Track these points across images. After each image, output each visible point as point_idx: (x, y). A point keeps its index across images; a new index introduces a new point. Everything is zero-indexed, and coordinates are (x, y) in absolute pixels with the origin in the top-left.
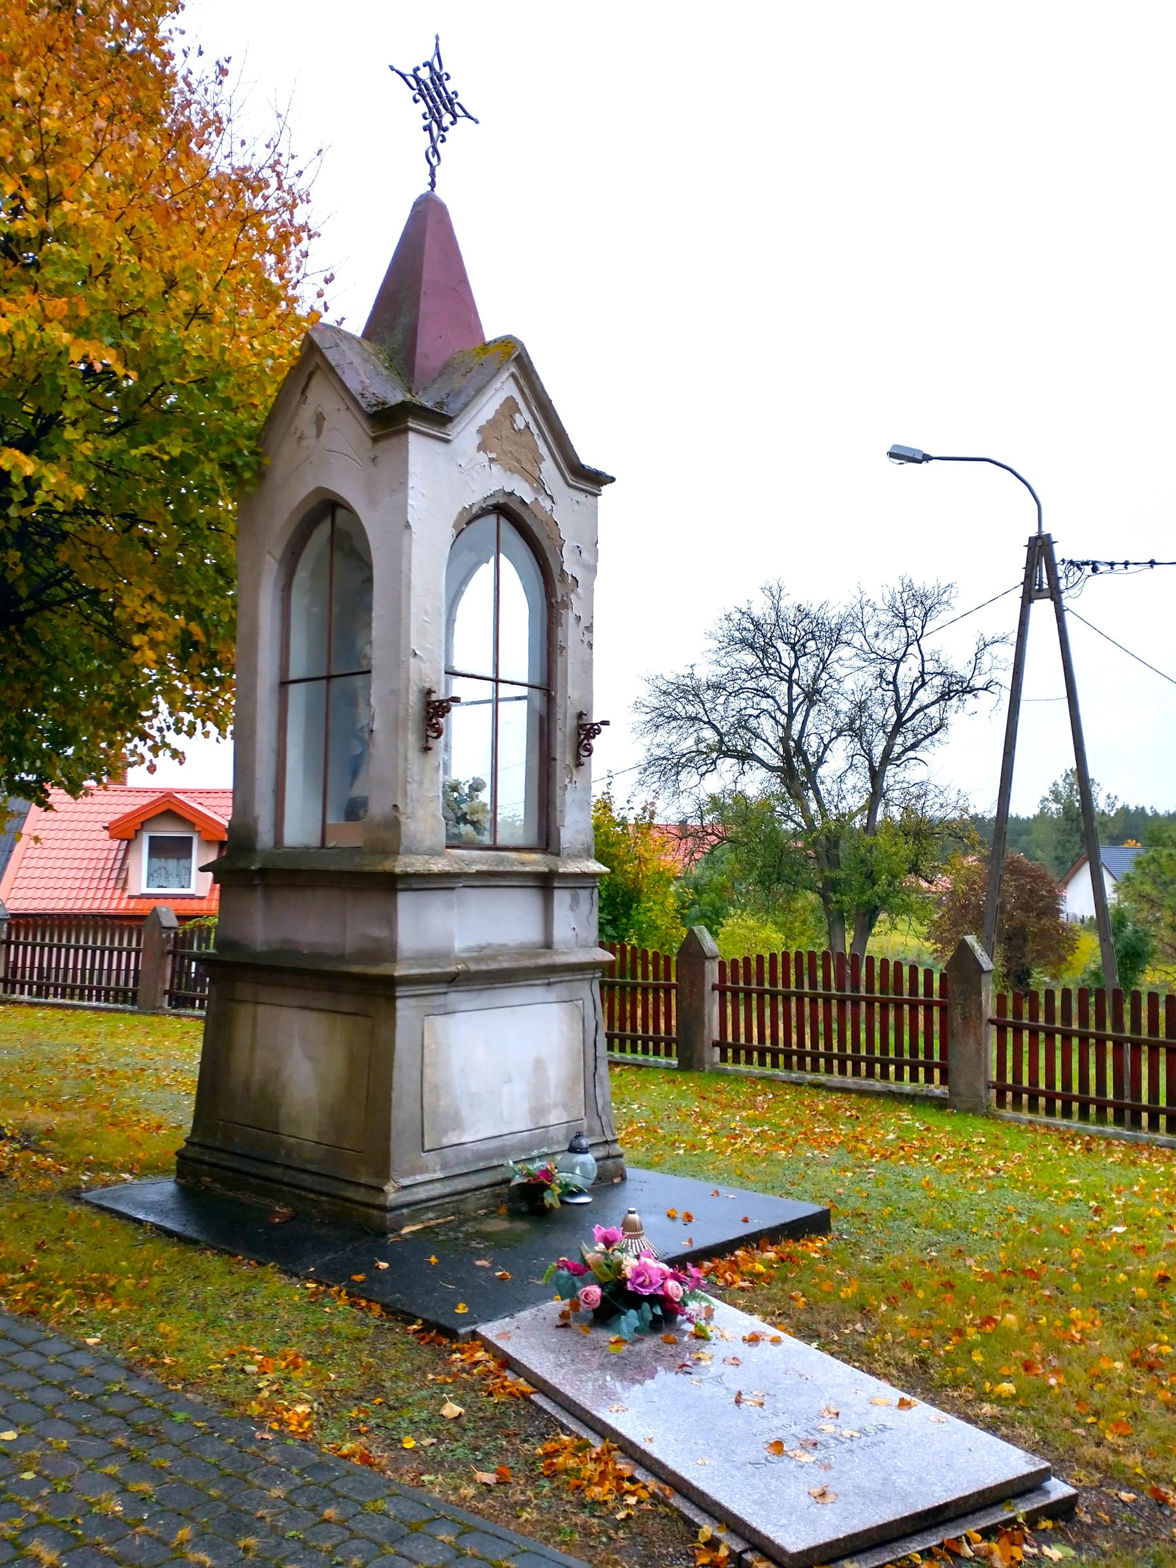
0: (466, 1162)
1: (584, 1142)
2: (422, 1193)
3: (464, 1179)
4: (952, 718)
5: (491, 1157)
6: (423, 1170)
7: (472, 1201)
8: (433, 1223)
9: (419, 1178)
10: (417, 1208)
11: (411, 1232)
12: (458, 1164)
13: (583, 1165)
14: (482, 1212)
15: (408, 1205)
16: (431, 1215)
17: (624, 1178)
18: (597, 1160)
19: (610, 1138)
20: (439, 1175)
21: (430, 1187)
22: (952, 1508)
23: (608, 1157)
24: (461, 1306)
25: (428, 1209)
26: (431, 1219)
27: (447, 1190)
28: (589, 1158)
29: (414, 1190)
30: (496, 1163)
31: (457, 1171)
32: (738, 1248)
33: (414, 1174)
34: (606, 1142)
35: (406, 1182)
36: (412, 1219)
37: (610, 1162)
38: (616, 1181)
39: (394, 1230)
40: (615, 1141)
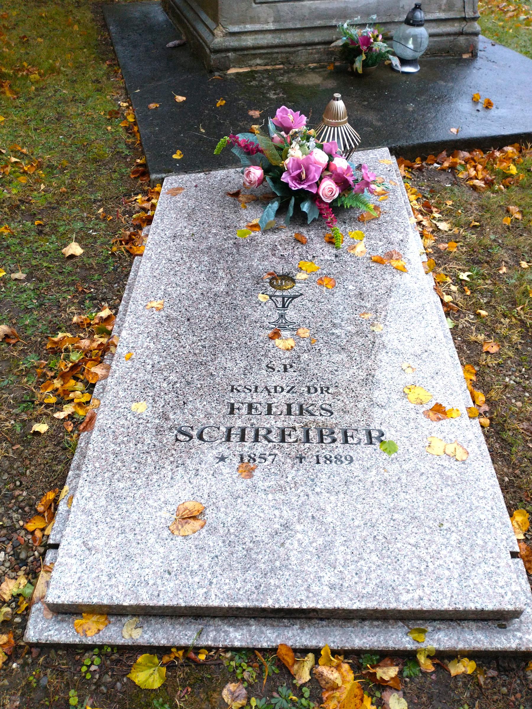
0: (302, 19)
1: (420, 15)
2: (249, 41)
3: (298, 34)
4: (409, 257)
5: (332, 17)
6: (253, 20)
7: (302, 55)
8: (259, 68)
9: (249, 27)
10: (244, 54)
11: (238, 74)
12: (293, 19)
13: (415, 38)
14: (312, 65)
15: (235, 50)
16: (258, 61)
17: (474, 55)
18: (431, 35)
19: (469, 14)
20: (271, 27)
21: (260, 36)
22: (427, 614)
23: (461, 34)
24: (175, 156)
25: (255, 56)
26: (258, 64)
27: (277, 41)
28: (422, 31)
29: (243, 37)
30: (334, 23)
31: (291, 25)
32: (511, 144)
33: (244, 23)
34: (464, 19)
35: (235, 29)
36: (239, 63)
37: (462, 39)
38: (465, 56)
39: (219, 69)
40: (474, 19)
